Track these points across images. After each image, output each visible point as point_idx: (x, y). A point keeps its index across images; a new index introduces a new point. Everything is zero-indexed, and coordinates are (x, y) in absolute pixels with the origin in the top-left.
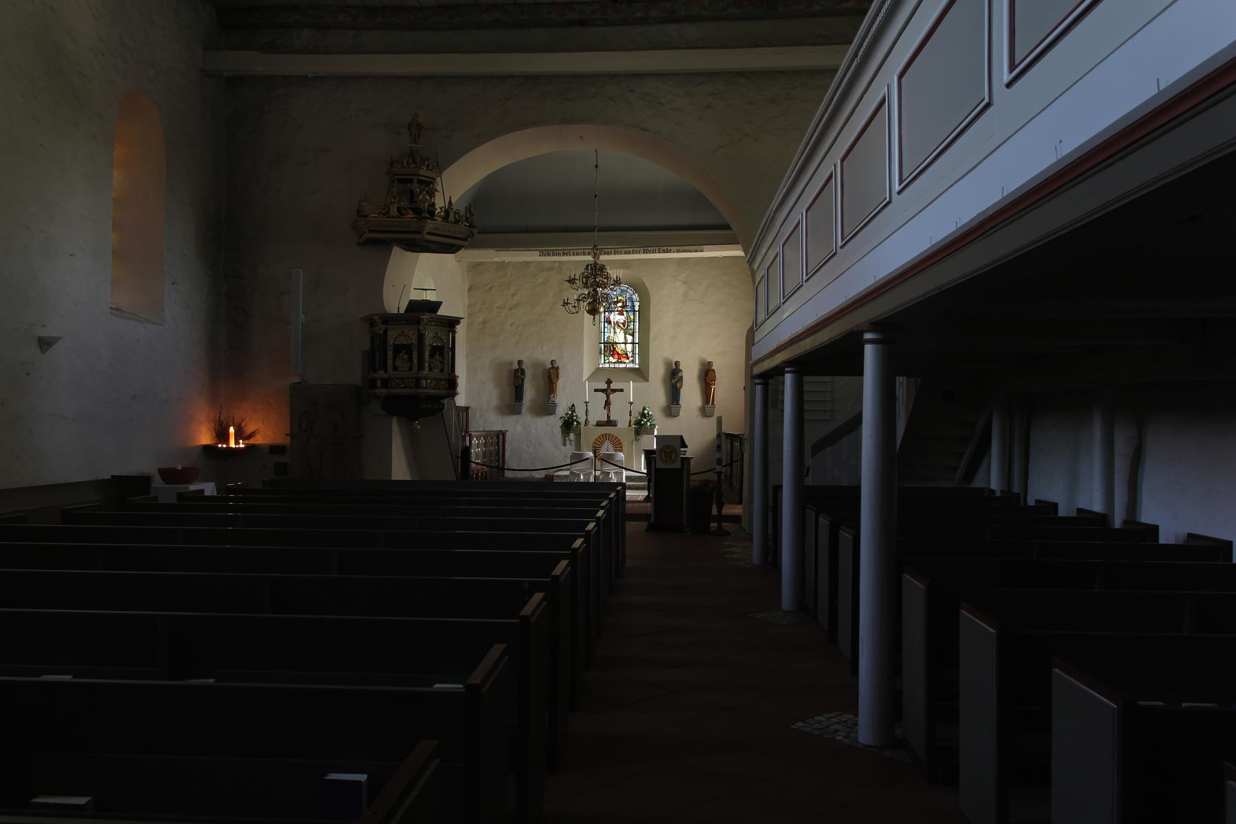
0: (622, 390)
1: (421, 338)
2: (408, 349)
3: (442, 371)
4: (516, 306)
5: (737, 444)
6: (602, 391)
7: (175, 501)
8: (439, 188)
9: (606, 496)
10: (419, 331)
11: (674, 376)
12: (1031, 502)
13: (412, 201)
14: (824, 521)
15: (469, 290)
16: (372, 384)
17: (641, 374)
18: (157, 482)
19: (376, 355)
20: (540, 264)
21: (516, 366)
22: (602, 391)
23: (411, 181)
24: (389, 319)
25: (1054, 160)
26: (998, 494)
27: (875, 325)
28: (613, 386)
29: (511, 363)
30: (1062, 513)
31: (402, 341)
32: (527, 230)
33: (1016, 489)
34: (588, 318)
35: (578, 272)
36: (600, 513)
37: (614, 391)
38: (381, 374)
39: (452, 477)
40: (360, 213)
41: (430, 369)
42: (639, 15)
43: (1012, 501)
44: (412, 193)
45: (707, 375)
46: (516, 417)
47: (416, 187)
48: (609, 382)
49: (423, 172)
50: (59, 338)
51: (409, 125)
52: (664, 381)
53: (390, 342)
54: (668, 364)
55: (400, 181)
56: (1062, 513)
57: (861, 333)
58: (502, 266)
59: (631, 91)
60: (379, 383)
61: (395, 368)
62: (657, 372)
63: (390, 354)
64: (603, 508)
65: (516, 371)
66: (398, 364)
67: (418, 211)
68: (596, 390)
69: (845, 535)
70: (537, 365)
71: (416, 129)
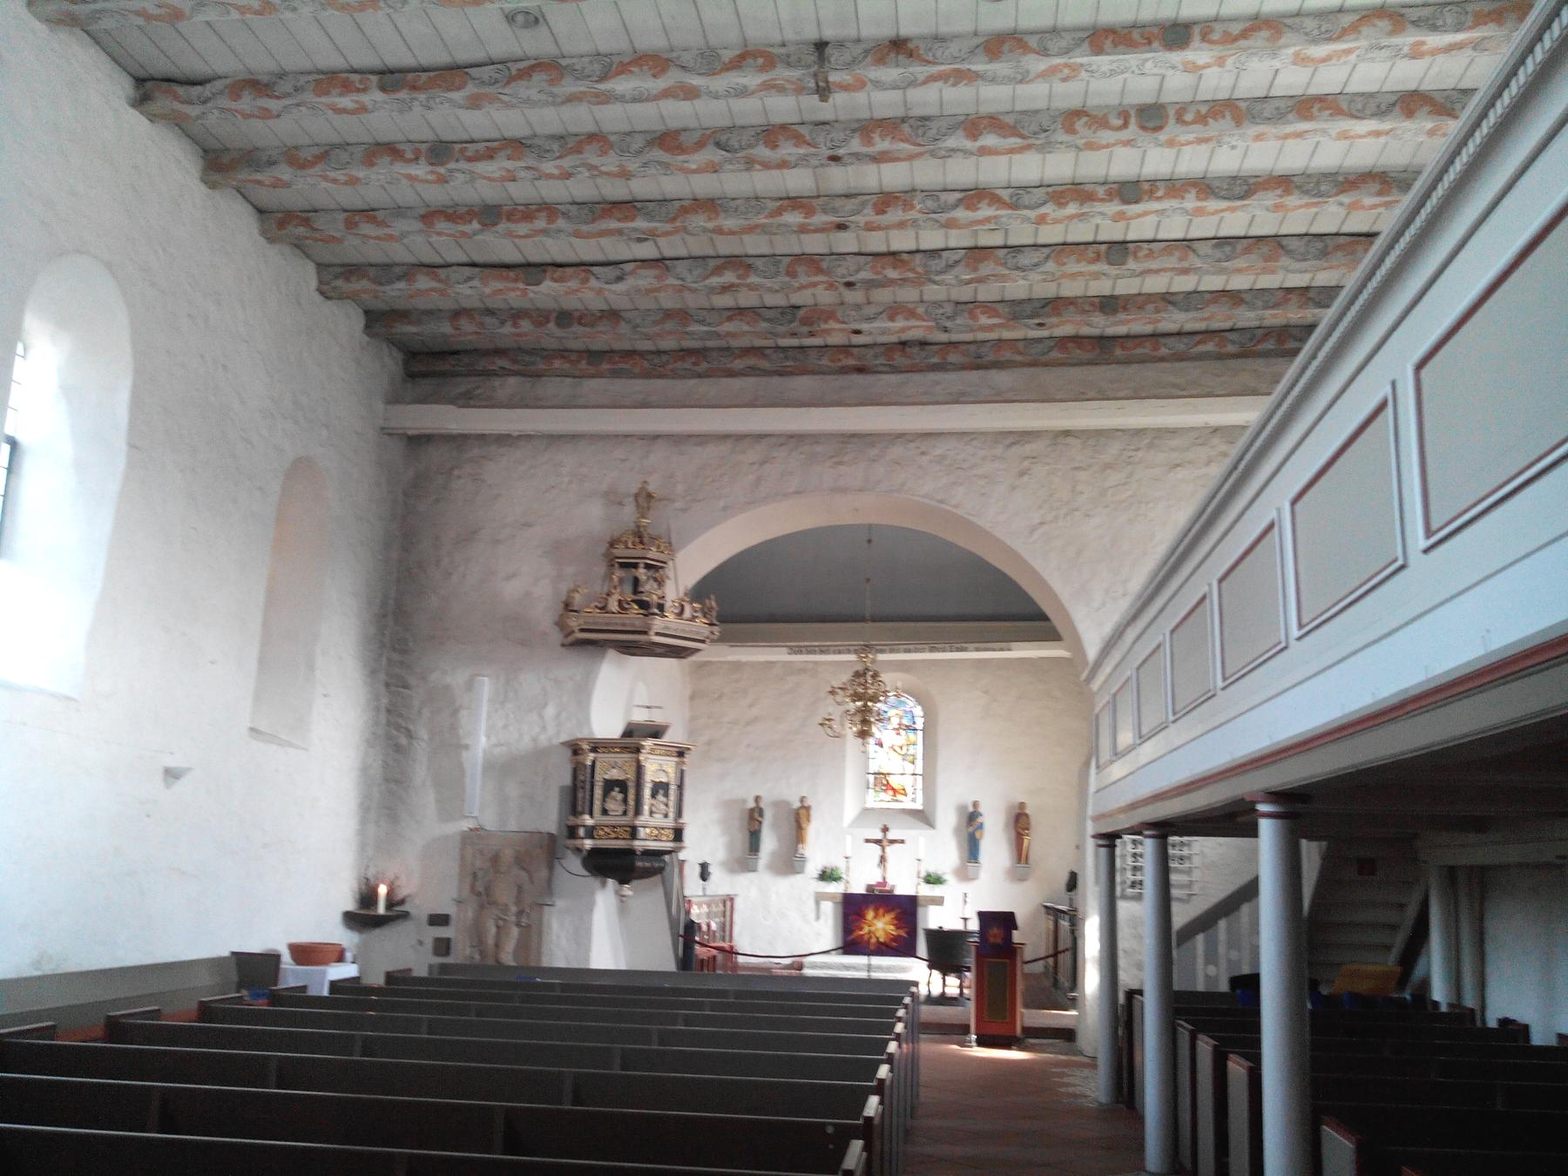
0: (902, 842)
1: (639, 770)
2: (622, 785)
3: (666, 816)
4: (755, 720)
5: (1065, 924)
6: (878, 842)
7: (325, 993)
8: (671, 574)
9: (899, 1001)
10: (638, 761)
11: (971, 820)
12: (1492, 1023)
13: (636, 592)
14: (1205, 1046)
15: (692, 698)
16: (572, 832)
17: (923, 817)
18: (286, 957)
19: (576, 796)
20: (785, 664)
21: (752, 804)
22: (878, 842)
23: (635, 566)
24: (597, 746)
25: (1480, 652)
26: (1444, 1009)
27: (1275, 796)
28: (891, 835)
29: (744, 801)
30: (1537, 1039)
31: (615, 774)
32: (773, 619)
33: (1469, 1001)
34: (852, 743)
35: (845, 677)
36: (899, 1028)
37: (892, 842)
38: (589, 821)
39: (670, 965)
40: (568, 606)
41: (651, 813)
42: (935, 360)
43: (1463, 1020)
44: (636, 582)
45: (1019, 822)
46: (750, 875)
47: (641, 573)
48: (885, 830)
49: (653, 553)
50: (189, 769)
51: (636, 496)
52: (957, 831)
53: (599, 777)
54: (961, 809)
55: (623, 566)
56: (1537, 1039)
57: (1254, 803)
58: (738, 666)
59: (923, 453)
60: (581, 832)
61: (605, 812)
62: (947, 819)
63: (598, 792)
64: (900, 1019)
65: (752, 811)
66: (610, 805)
67: (644, 605)
68: (868, 841)
69: (1237, 1068)
70: (780, 805)
71: (645, 499)
